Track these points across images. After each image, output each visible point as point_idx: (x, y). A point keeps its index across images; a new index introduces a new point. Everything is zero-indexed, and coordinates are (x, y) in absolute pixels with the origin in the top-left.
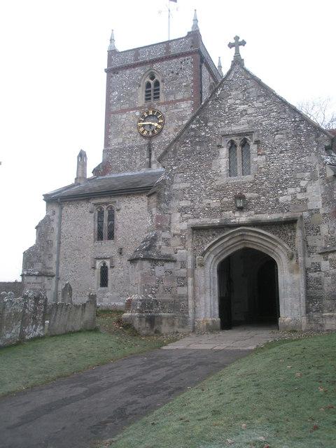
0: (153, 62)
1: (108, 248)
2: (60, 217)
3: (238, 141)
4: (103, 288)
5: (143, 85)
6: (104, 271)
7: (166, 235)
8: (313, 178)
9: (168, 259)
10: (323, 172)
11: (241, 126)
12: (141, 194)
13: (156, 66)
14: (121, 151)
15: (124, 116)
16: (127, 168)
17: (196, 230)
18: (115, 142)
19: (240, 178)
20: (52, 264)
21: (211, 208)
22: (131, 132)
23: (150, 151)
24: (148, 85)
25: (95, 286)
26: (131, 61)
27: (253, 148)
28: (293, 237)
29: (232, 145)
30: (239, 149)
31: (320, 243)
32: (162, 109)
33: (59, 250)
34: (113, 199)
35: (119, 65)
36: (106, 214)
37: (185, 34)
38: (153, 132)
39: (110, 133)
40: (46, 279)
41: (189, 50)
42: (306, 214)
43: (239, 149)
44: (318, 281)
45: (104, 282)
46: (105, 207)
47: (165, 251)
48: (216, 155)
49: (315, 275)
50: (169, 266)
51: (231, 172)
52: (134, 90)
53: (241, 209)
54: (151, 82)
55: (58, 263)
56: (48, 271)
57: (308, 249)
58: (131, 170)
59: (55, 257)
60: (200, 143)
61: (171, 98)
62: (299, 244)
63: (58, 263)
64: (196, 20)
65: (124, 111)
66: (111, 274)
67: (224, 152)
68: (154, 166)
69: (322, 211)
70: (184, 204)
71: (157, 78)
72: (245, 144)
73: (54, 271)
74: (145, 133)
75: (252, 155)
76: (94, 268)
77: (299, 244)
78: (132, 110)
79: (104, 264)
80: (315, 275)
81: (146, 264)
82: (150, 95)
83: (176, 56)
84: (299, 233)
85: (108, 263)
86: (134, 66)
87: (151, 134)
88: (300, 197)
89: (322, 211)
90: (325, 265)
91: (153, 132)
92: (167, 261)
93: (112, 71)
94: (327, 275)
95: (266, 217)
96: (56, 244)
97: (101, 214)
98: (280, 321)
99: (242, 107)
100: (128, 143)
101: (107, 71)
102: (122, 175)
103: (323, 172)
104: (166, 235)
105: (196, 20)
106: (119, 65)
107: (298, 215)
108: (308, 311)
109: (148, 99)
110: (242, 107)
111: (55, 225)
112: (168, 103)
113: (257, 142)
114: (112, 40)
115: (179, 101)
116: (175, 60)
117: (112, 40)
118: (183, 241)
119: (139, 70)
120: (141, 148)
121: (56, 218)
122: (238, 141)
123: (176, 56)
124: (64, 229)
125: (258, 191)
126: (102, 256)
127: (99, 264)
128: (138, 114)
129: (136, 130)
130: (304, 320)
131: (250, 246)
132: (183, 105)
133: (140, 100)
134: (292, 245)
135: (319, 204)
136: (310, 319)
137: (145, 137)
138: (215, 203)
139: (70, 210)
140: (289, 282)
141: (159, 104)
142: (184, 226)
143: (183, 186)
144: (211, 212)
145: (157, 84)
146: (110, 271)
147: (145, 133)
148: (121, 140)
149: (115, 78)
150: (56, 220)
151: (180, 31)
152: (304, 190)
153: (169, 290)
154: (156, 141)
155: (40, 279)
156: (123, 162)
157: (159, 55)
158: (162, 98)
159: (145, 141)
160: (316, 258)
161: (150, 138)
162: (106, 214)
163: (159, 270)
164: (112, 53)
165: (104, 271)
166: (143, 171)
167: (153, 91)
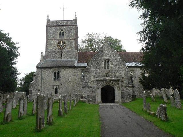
0: (63, 26)
1: (57, 83)
2: (42, 73)
3: (107, 61)
4: (56, 94)
5: (59, 32)
6: (56, 89)
7: (90, 81)
8: (123, 71)
9: (91, 87)
10: (125, 70)
11: (107, 57)
12: (68, 68)
13: (64, 27)
14: (52, 52)
15: (53, 41)
16: (54, 58)
17: (97, 80)
18: (50, 49)
19: (107, 69)
20: (39, 87)
21: (101, 76)
22: (55, 47)
23: (61, 53)
24: (60, 33)
25: (54, 94)
26: (55, 24)
27: (110, 63)
28: (119, 83)
29: (105, 62)
30: (107, 62)
31: (124, 85)
32: (65, 41)
33: (41, 83)
34: (59, 69)
35: (51, 25)
36: (57, 73)
37: (73, 19)
38: (62, 47)
39: (48, 46)
40: (38, 91)
41: (74, 24)
42: (121, 78)
43: (107, 62)
44: (123, 92)
45: (56, 92)
46: (57, 71)
47: (90, 85)
48: (101, 63)
49: (123, 91)
50: (91, 89)
51: (105, 68)
52: (56, 34)
53: (107, 76)
54: (62, 32)
55: (41, 87)
56: (38, 89)
57: (122, 86)
58: (56, 59)
59: (40, 85)
60: (98, 60)
61: (68, 38)
62: (120, 85)
63: (41, 87)
64: (76, 16)
65: (52, 40)
66: (58, 90)
67: (103, 63)
68: (63, 58)
69: (125, 78)
70: (94, 74)
71: (63, 31)
72: (108, 62)
73: (40, 89)
74: (60, 48)
75: (110, 64)
76: (53, 88)
77: (120, 85)
78: (55, 40)
79: (56, 87)
80: (123, 91)
81: (87, 88)
82: (61, 35)
83: (70, 26)
84: (120, 82)
85: (58, 87)
86: (56, 26)
87: (61, 48)
88: (120, 75)
89: (125, 78)
90: (125, 89)
91: (62, 47)
92: (91, 87)
93: (48, 26)
94: (125, 91)
95: (113, 78)
96: (40, 81)
97: (55, 74)
98: (115, 101)
99: (107, 53)
100: (54, 50)
101: (46, 26)
102: (52, 60)
103: (125, 70)
104: (90, 81)
105: (76, 16)
106: (51, 25)
107: (119, 78)
108: (122, 99)
109: (60, 37)
110: (107, 53)
111: (40, 75)
112: (67, 39)
113: (111, 62)
114: (48, 16)
115: (71, 39)
116: (70, 27)
117: (48, 16)
118: (94, 83)
119: (57, 28)
120: (58, 52)
121: (40, 73)
122: (107, 61)
123: (70, 26)
124: (43, 76)
125: (111, 73)
126: (55, 85)
127: (55, 87)
128: (57, 41)
129: (57, 46)
130: (121, 100)
131: (109, 85)
132: (72, 41)
133: (58, 37)
134: (118, 85)
135: (124, 76)
136: (122, 100)
137: (59, 49)
138: (101, 75)
139: (45, 71)
140: (117, 93)
141: (64, 39)
142: (94, 79)
143: (94, 70)
144: (101, 76)
145: (63, 33)
146: (58, 89)
147: (60, 48)
148: (51, 49)
149: (49, 29)
150: (40, 74)
151: (70, 17)
152: (121, 73)
153: (91, 94)
154: (63, 51)
155: (36, 91)
156: (52, 56)
157: (64, 24)
158: (65, 37)
159: (59, 50)
160: (123, 88)
161: (61, 49)
162: (57, 73)
163: (89, 90)
164: (48, 21)
165: (56, 89)
166: (59, 59)
167: (62, 35)
